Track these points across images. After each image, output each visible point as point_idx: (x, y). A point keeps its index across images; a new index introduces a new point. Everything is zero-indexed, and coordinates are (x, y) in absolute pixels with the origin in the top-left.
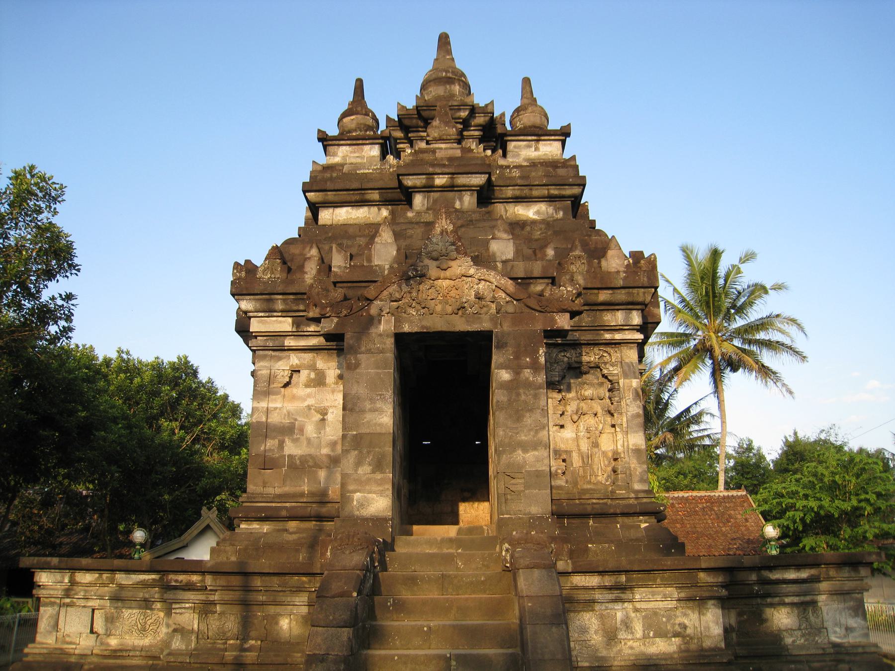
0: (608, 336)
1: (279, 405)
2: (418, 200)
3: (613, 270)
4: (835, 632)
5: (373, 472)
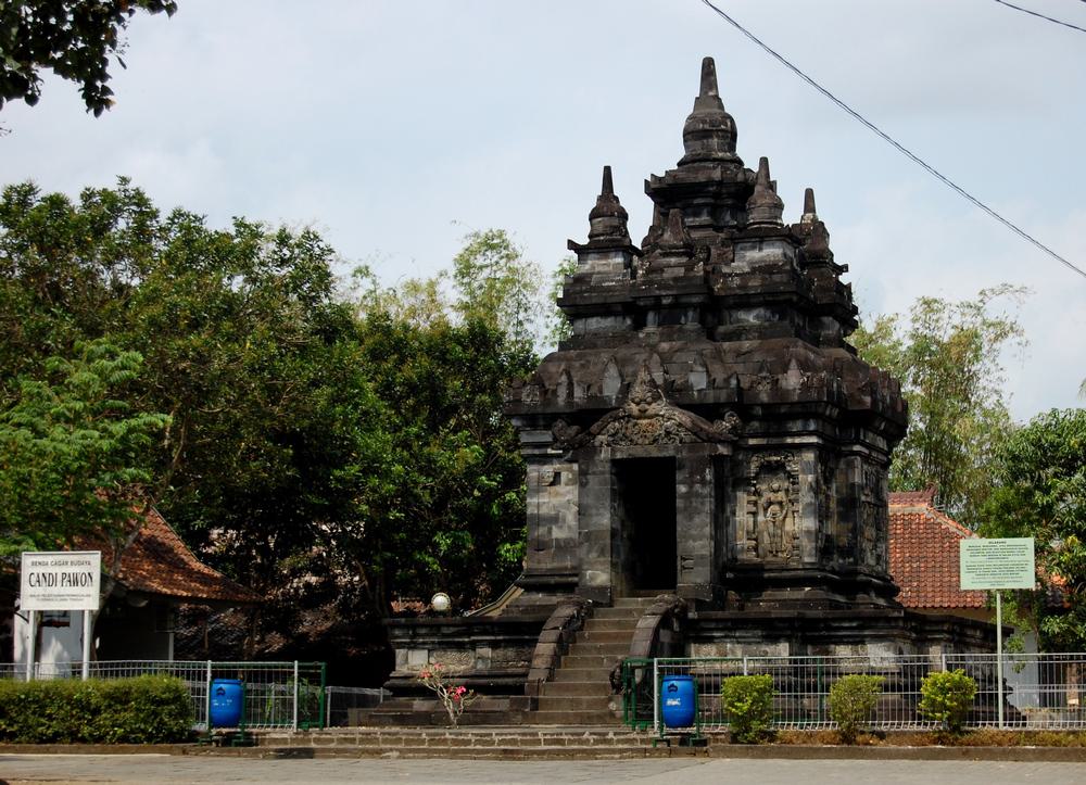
0: (789, 440)
1: (546, 500)
3: (791, 388)
5: (599, 556)
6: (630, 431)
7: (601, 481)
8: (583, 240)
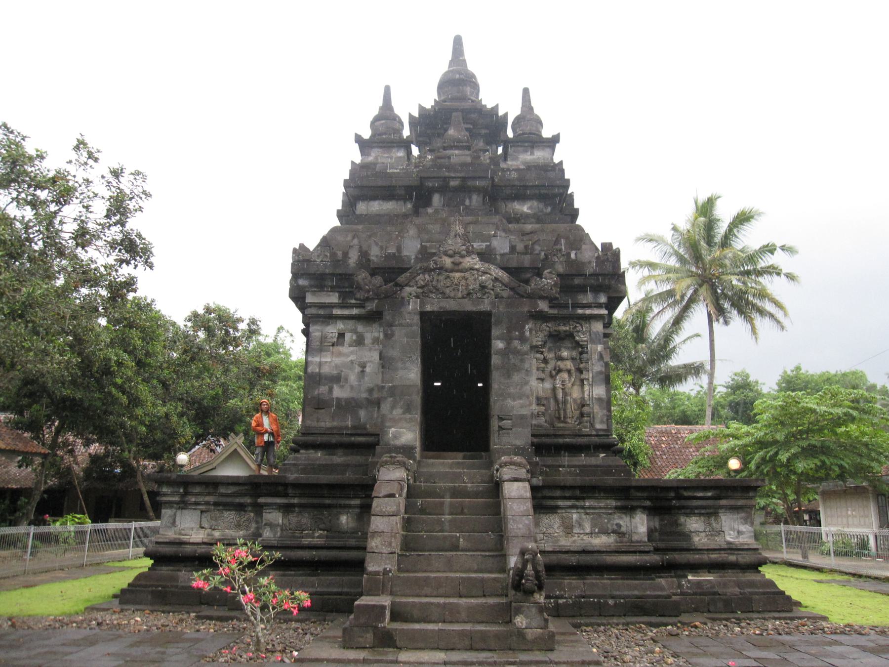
0: (580, 311)
1: (329, 360)
2: (436, 199)
4: (730, 534)
5: (404, 413)
6: (442, 284)
7: (407, 334)
8: (367, 134)
